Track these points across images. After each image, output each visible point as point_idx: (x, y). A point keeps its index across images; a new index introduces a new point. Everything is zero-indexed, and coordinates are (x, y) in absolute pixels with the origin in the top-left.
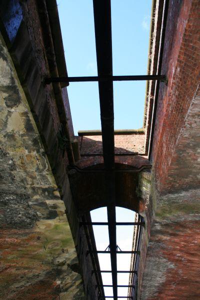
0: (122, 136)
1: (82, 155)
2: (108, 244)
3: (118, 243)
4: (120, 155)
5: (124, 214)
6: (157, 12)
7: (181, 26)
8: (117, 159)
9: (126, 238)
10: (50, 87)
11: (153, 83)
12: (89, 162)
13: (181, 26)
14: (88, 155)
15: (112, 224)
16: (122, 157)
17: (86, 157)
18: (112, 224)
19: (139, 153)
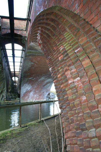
0: (18, 20)
1: (2, 29)
2: (12, 54)
3: (15, 54)
4: (17, 30)
5: (18, 47)
6: (31, 7)
7: (44, 5)
8: (15, 32)
9: (18, 54)
10: (3, 50)
11: (29, 18)
12: (5, 32)
13: (44, 5)
14: (5, 29)
15: (13, 50)
16: (17, 31)
17: (4, 29)
18: (13, 50)
19: (23, 30)
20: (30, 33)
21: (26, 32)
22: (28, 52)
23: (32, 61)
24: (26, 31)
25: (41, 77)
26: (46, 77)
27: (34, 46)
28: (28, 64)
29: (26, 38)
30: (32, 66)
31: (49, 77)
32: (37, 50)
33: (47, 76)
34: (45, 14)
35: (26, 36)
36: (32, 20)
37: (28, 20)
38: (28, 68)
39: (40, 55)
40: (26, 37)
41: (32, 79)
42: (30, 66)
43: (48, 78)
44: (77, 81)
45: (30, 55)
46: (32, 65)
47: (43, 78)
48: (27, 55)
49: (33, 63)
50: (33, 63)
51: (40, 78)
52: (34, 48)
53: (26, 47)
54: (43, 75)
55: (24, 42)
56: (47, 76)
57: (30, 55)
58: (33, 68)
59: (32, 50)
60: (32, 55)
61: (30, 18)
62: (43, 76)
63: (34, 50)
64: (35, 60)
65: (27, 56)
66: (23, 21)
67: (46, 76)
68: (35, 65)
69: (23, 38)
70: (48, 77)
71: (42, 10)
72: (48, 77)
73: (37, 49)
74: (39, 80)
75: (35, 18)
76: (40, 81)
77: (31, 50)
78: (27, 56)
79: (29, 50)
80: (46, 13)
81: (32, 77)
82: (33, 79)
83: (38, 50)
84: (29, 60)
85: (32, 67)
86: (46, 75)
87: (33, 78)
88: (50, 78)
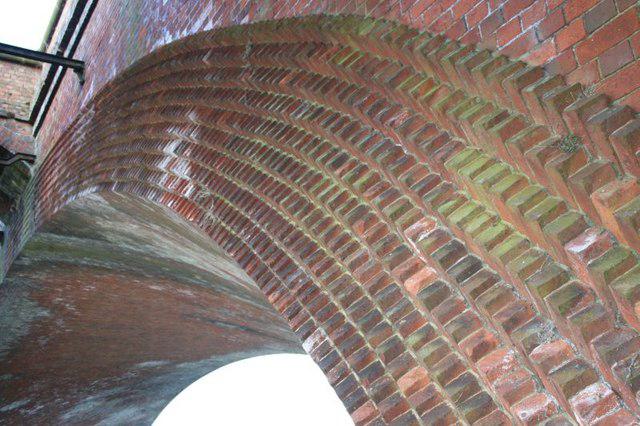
19: (17, 116)
20: (79, 136)
21: (29, 130)
22: (39, 247)
23: (43, 301)
24: (31, 122)
25: (77, 400)
26: (110, 398)
27: (92, 213)
28: (16, 316)
29: (32, 162)
30: (40, 328)
31: (126, 395)
32: (99, 238)
33: (117, 390)
34: (248, 50)
35: (28, 151)
36: (105, 71)
37: (60, 61)
38: (9, 339)
39: (107, 265)
40: (31, 159)
41: (22, 411)
42: (25, 332)
43: (118, 401)
44: (595, 405)
45: (44, 265)
46: (38, 320)
47: (87, 406)
48: (26, 261)
49: (45, 313)
50: (45, 313)
51: (71, 400)
52: (85, 224)
53: (28, 212)
54: (97, 386)
55: (9, 185)
56: (117, 390)
57: (44, 265)
58: (42, 341)
59: (70, 234)
60: (60, 264)
61: (78, 56)
62: (90, 393)
63: (81, 236)
64: (64, 294)
65: (21, 268)
66: (16, 66)
67: (110, 392)
68: (60, 322)
69: (9, 162)
70: (119, 396)
71: (210, 26)
72: (119, 396)
73: (104, 230)
74: (67, 416)
75: (130, 61)
76: (69, 421)
77: (60, 233)
78: (21, 268)
79: (44, 235)
80: (249, 42)
81: (28, 395)
82: (31, 412)
83: (110, 237)
84: (25, 294)
85: (34, 335)
86: (113, 385)
87: (30, 406)
88: (130, 401)
